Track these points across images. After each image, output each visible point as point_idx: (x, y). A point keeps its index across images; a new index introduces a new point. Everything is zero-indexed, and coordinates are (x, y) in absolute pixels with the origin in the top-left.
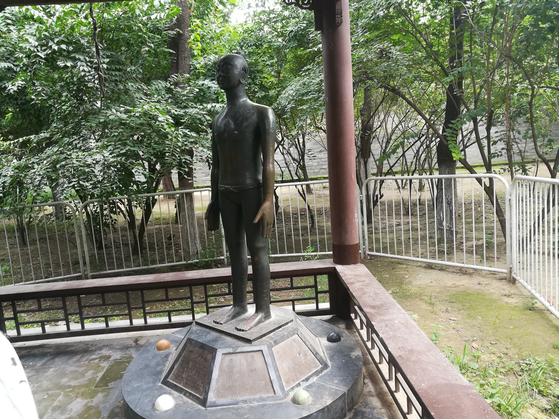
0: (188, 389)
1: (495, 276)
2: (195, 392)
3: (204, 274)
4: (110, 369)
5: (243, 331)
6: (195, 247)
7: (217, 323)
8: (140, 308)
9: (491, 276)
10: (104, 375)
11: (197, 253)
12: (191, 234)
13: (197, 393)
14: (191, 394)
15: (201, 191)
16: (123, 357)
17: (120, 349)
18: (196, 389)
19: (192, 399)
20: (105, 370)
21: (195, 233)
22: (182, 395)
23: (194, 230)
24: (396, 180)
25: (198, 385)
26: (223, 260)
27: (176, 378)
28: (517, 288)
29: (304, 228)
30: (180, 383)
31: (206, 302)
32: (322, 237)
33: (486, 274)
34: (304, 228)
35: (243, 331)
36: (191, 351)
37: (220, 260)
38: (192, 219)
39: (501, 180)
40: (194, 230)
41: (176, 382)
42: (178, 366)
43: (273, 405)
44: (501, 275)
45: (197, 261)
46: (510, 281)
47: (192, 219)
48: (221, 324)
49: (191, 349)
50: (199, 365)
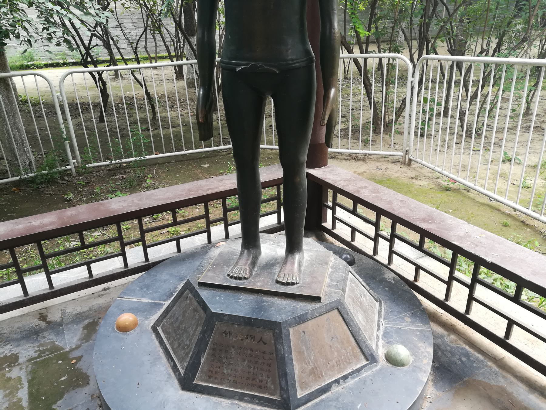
0: (244, 389)
1: (386, 159)
2: (259, 392)
3: (136, 201)
4: (33, 379)
5: (293, 284)
6: (25, 157)
7: (240, 278)
8: (38, 268)
9: (383, 159)
10: (30, 394)
11: (30, 164)
12: (15, 139)
13: (264, 393)
14: (253, 397)
15: (22, 76)
16: (43, 352)
17: (23, 338)
18: (260, 387)
19: (258, 404)
20: (26, 385)
21: (21, 137)
22: (236, 402)
23: (19, 132)
24: (91, 73)
25: (261, 381)
26: (71, 169)
27: (210, 377)
28: (414, 169)
29: (144, 121)
30: (221, 384)
31: (142, 240)
32: (157, 131)
33: (377, 158)
34: (144, 121)
35: (293, 284)
36: (225, 332)
37: (66, 170)
38: (13, 116)
39: (402, 59)
40: (19, 132)
41: (213, 383)
42: (207, 359)
43: (374, 375)
44: (391, 157)
45: (33, 175)
46: (404, 163)
47: (13, 116)
48: (246, 279)
49: (224, 329)
50: (251, 350)
